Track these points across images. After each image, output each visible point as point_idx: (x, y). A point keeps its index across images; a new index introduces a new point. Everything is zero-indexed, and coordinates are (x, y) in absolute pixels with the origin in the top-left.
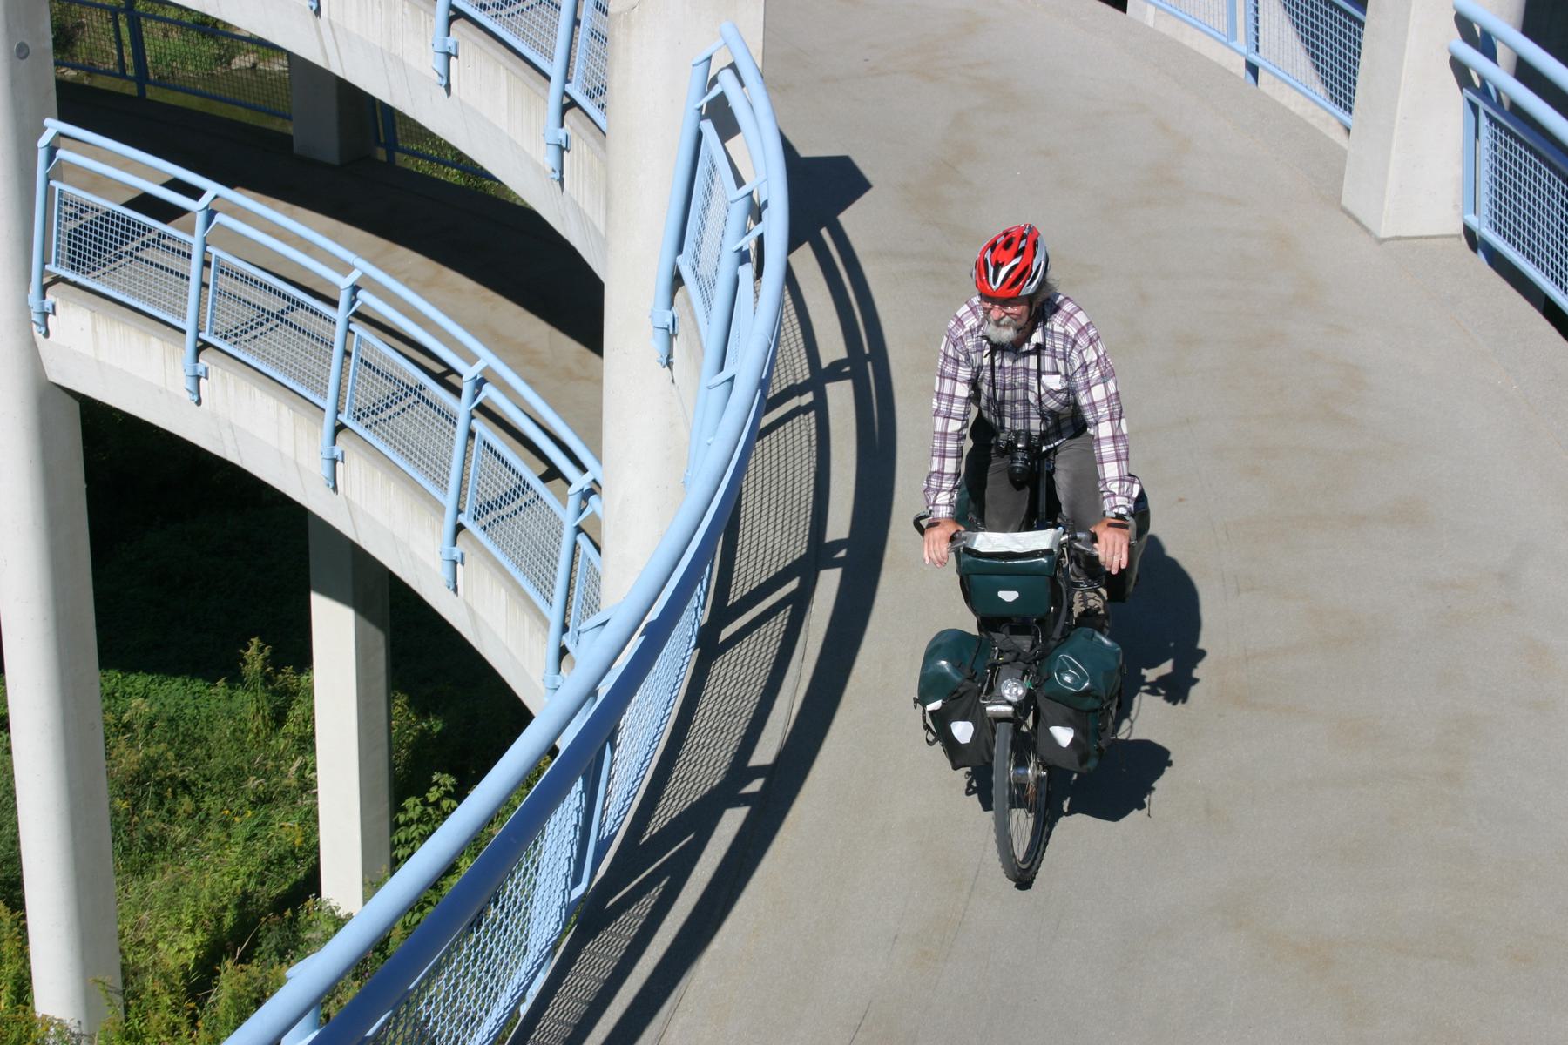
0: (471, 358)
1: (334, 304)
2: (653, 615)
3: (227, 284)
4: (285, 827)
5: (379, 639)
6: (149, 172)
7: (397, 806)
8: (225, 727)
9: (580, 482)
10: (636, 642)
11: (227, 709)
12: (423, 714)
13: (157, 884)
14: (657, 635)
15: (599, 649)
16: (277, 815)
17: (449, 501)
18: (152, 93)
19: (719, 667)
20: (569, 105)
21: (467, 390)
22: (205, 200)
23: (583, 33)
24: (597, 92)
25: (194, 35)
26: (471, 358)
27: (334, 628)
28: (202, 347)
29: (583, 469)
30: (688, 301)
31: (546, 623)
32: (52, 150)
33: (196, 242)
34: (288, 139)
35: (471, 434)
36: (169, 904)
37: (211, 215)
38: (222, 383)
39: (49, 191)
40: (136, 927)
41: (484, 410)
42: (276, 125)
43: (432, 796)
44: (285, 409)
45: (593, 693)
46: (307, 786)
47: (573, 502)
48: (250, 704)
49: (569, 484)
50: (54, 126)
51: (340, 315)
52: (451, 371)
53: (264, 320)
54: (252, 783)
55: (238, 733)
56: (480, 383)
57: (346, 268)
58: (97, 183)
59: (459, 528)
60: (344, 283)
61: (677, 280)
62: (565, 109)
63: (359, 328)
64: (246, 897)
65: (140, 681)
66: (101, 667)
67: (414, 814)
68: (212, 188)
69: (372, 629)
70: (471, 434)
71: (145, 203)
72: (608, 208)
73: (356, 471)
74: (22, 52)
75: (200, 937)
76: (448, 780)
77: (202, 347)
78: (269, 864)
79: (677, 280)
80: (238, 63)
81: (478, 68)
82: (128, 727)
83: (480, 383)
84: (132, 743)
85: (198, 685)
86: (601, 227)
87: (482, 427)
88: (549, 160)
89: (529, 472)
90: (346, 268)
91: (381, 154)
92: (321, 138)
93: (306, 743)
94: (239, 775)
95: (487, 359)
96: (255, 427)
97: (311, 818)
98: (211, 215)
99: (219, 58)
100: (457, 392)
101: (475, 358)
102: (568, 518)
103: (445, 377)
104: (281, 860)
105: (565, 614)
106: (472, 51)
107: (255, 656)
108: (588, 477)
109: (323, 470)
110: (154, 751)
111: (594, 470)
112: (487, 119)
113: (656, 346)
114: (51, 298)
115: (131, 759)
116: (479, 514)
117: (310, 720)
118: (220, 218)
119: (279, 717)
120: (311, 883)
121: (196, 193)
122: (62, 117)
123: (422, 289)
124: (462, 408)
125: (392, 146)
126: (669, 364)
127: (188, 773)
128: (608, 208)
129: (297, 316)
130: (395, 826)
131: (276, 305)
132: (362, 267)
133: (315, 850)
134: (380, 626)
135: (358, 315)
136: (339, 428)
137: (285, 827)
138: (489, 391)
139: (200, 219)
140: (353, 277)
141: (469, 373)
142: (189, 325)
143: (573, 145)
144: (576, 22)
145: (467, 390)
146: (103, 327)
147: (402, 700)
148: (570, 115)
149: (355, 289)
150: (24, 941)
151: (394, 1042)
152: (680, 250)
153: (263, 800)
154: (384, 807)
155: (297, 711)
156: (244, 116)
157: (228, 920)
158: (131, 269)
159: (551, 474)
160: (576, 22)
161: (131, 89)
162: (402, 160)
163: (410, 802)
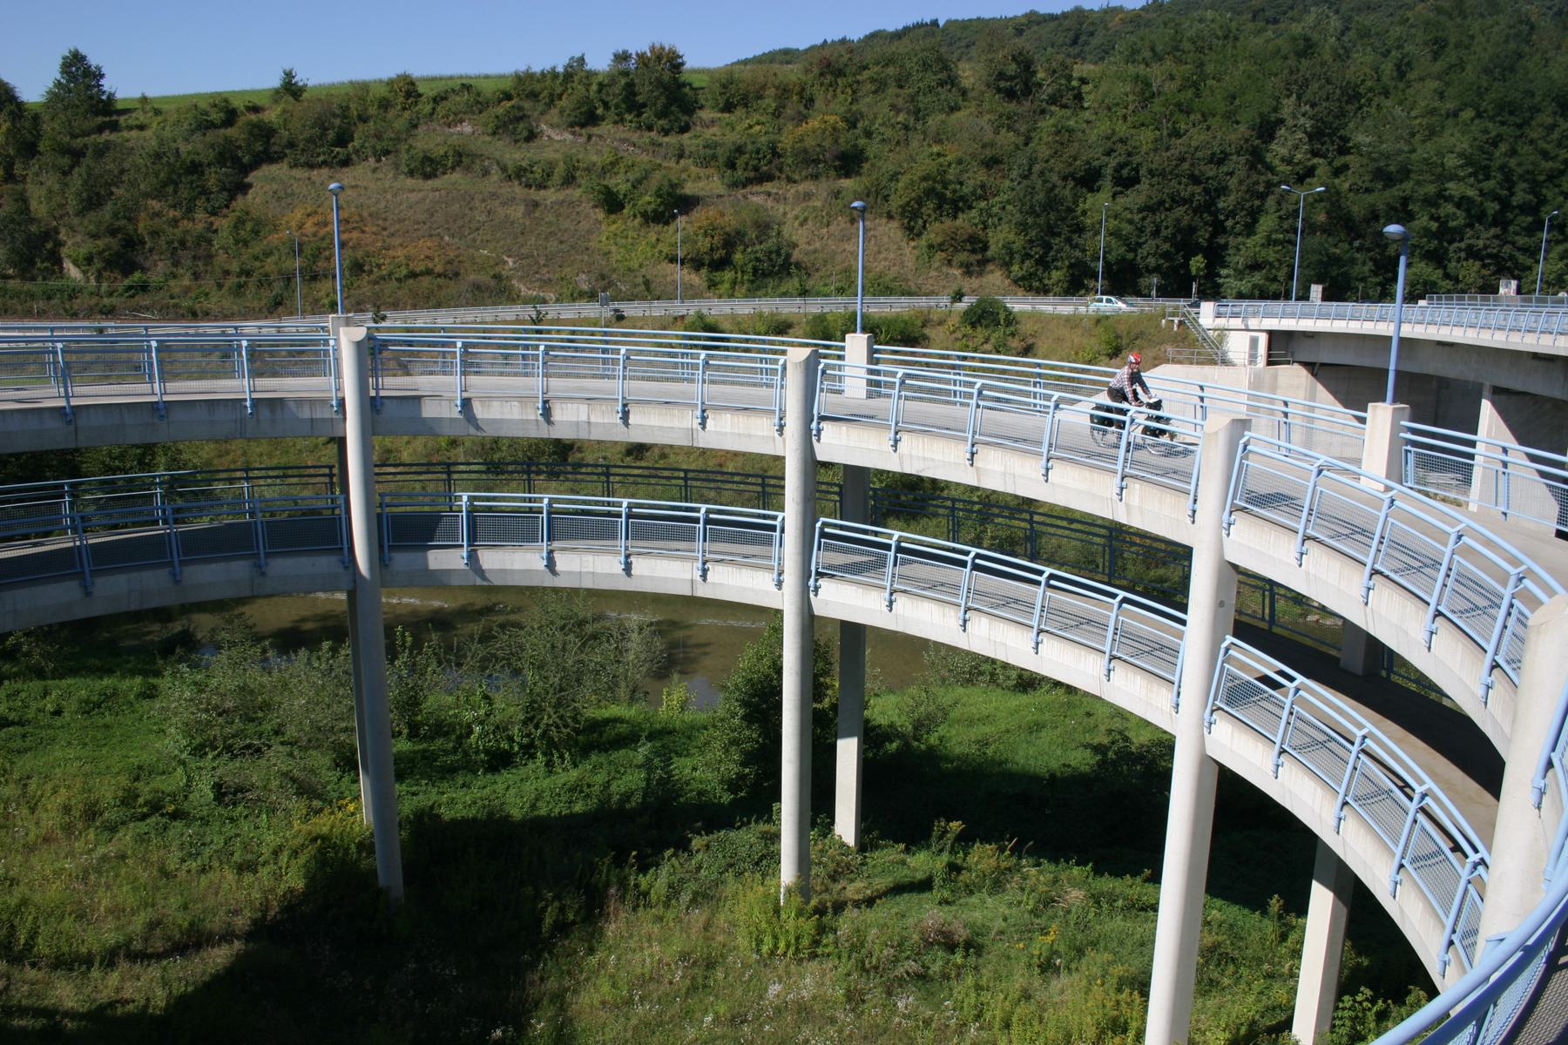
0: (1421, 782)
1: (1352, 743)
2: (1530, 943)
3: (1299, 724)
4: (1278, 993)
5: (1344, 911)
6: (1268, 665)
7: (1339, 998)
8: (1256, 935)
9: (1473, 857)
10: (1519, 954)
11: (1259, 927)
12: (1359, 954)
13: (1211, 1003)
14: (1529, 953)
15: (1488, 958)
16: (1276, 986)
17: (1398, 852)
18: (1275, 630)
19: (1556, 977)
20: (1495, 666)
21: (1416, 798)
22: (1295, 683)
23: (1508, 632)
24: (1515, 662)
25: (1290, 603)
26: (1421, 782)
27: (1321, 900)
28: (1282, 751)
29: (1476, 851)
30: (1555, 776)
31: (1444, 927)
32: (1227, 649)
33: (1288, 702)
34: (1338, 660)
35: (1415, 821)
36: (1215, 1014)
37: (1297, 690)
38: (1289, 771)
39: (1222, 668)
40: (1198, 1021)
41: (1423, 810)
42: (1333, 652)
43: (1359, 998)
44: (1319, 789)
45: (1488, 978)
46: (1293, 975)
47: (1468, 866)
48: (1270, 927)
49: (1466, 857)
50: (1230, 639)
51: (1355, 749)
52: (1408, 785)
53: (1315, 745)
54: (1266, 966)
55: (1263, 939)
56: (1424, 796)
57: (1360, 727)
58: (1244, 667)
59: (1402, 866)
60: (1359, 734)
61: (1550, 765)
62: (1493, 668)
63: (1362, 756)
64: (1253, 1022)
65: (1218, 902)
66: (1207, 891)
67: (1347, 1005)
68: (1300, 679)
69: (1341, 905)
70: (1415, 821)
71: (1265, 679)
72: (1514, 721)
73: (1351, 826)
74: (1221, 604)
75: (1227, 1035)
76: (1368, 993)
77: (1282, 751)
78: (1267, 1009)
79: (1550, 765)
80: (1310, 618)
81: (1447, 641)
82: (1209, 923)
83: (1424, 796)
84: (1210, 932)
85: (1246, 911)
86: (1507, 730)
87: (1421, 817)
88: (1481, 692)
89: (1445, 846)
90: (1360, 727)
91: (1384, 673)
92: (1355, 662)
93: (1297, 954)
94: (1260, 962)
95: (1430, 784)
96: (1302, 794)
97: (1293, 992)
98: (1297, 690)
99: (1301, 615)
100: (1411, 799)
101: (1424, 783)
102: (1465, 873)
103: (1405, 787)
104: (1274, 1008)
105: (1455, 924)
106: (1445, 633)
107: (1275, 903)
108: (1479, 856)
109: (1334, 822)
110: (1220, 938)
111: (1483, 853)
112: (1452, 669)
113: (1533, 797)
114: (1214, 716)
115: (1209, 940)
116: (1414, 860)
117: (1301, 942)
118: (1301, 693)
119: (1283, 937)
120: (1288, 1024)
121: (1292, 679)
122: (1235, 635)
123: (1398, 742)
124: (1412, 807)
125: (1390, 670)
126: (1539, 808)
127: (1236, 954)
128: (1514, 721)
129: (1331, 745)
130: (1337, 1008)
131: (1321, 738)
132: (1369, 727)
133: (1293, 1008)
134: (1345, 904)
135: (1363, 751)
136: (1345, 803)
137: (1278, 993)
138: (1428, 800)
139: (1292, 692)
140: (1364, 732)
141: (1419, 789)
142: (1278, 740)
143: (1496, 685)
144: (1505, 627)
145: (1416, 798)
146: (1236, 734)
147: (1348, 944)
148: (1495, 671)
149: (1364, 737)
150: (1146, 1011)
151: (18, 363)
152: (1553, 750)
153: (1269, 976)
154: (1332, 997)
155: (1292, 937)
156: (1308, 642)
157: (1243, 1030)
158: (1254, 709)
159: (1456, 848)
160: (1505, 627)
161: (1264, 625)
162: (1394, 678)
163: (1346, 998)
